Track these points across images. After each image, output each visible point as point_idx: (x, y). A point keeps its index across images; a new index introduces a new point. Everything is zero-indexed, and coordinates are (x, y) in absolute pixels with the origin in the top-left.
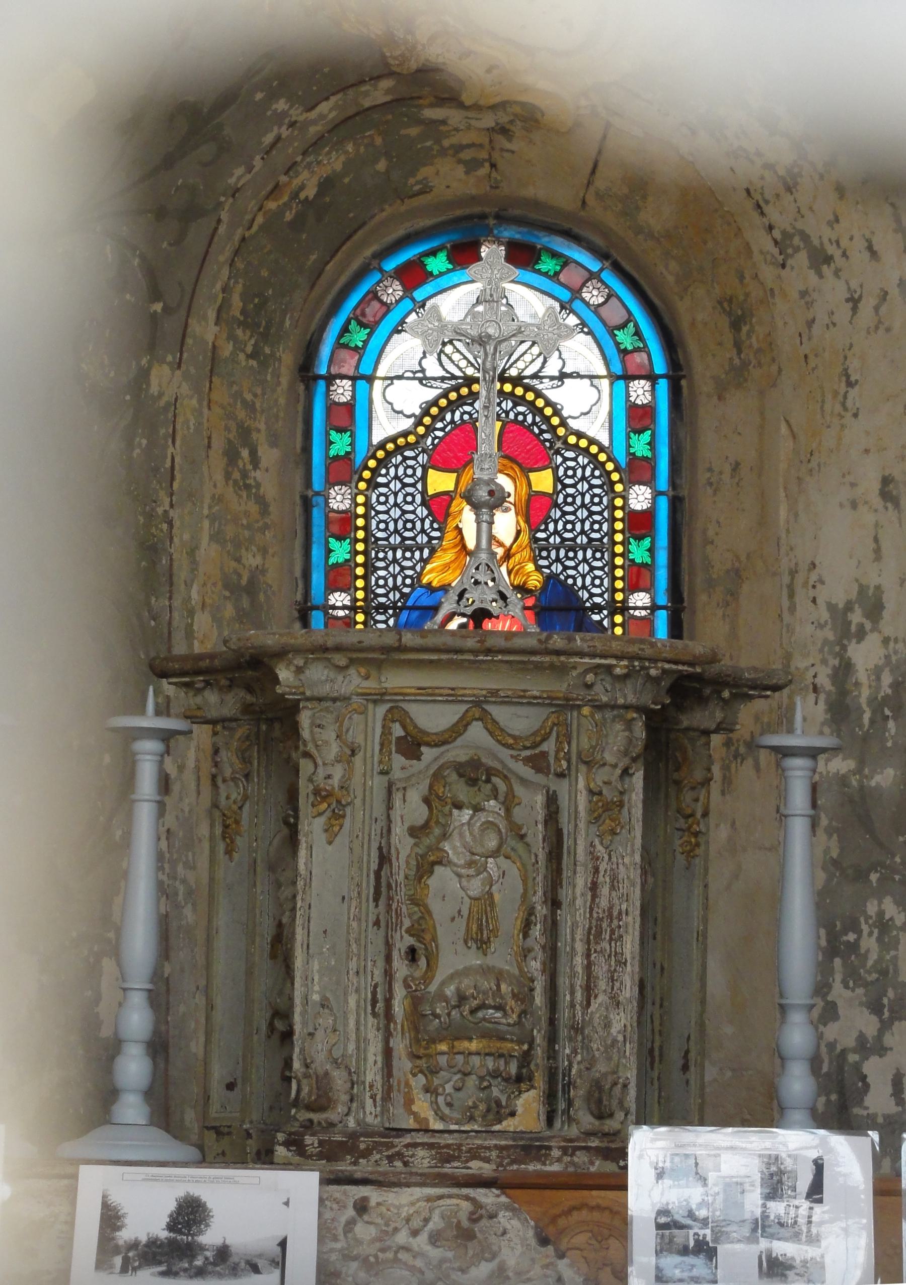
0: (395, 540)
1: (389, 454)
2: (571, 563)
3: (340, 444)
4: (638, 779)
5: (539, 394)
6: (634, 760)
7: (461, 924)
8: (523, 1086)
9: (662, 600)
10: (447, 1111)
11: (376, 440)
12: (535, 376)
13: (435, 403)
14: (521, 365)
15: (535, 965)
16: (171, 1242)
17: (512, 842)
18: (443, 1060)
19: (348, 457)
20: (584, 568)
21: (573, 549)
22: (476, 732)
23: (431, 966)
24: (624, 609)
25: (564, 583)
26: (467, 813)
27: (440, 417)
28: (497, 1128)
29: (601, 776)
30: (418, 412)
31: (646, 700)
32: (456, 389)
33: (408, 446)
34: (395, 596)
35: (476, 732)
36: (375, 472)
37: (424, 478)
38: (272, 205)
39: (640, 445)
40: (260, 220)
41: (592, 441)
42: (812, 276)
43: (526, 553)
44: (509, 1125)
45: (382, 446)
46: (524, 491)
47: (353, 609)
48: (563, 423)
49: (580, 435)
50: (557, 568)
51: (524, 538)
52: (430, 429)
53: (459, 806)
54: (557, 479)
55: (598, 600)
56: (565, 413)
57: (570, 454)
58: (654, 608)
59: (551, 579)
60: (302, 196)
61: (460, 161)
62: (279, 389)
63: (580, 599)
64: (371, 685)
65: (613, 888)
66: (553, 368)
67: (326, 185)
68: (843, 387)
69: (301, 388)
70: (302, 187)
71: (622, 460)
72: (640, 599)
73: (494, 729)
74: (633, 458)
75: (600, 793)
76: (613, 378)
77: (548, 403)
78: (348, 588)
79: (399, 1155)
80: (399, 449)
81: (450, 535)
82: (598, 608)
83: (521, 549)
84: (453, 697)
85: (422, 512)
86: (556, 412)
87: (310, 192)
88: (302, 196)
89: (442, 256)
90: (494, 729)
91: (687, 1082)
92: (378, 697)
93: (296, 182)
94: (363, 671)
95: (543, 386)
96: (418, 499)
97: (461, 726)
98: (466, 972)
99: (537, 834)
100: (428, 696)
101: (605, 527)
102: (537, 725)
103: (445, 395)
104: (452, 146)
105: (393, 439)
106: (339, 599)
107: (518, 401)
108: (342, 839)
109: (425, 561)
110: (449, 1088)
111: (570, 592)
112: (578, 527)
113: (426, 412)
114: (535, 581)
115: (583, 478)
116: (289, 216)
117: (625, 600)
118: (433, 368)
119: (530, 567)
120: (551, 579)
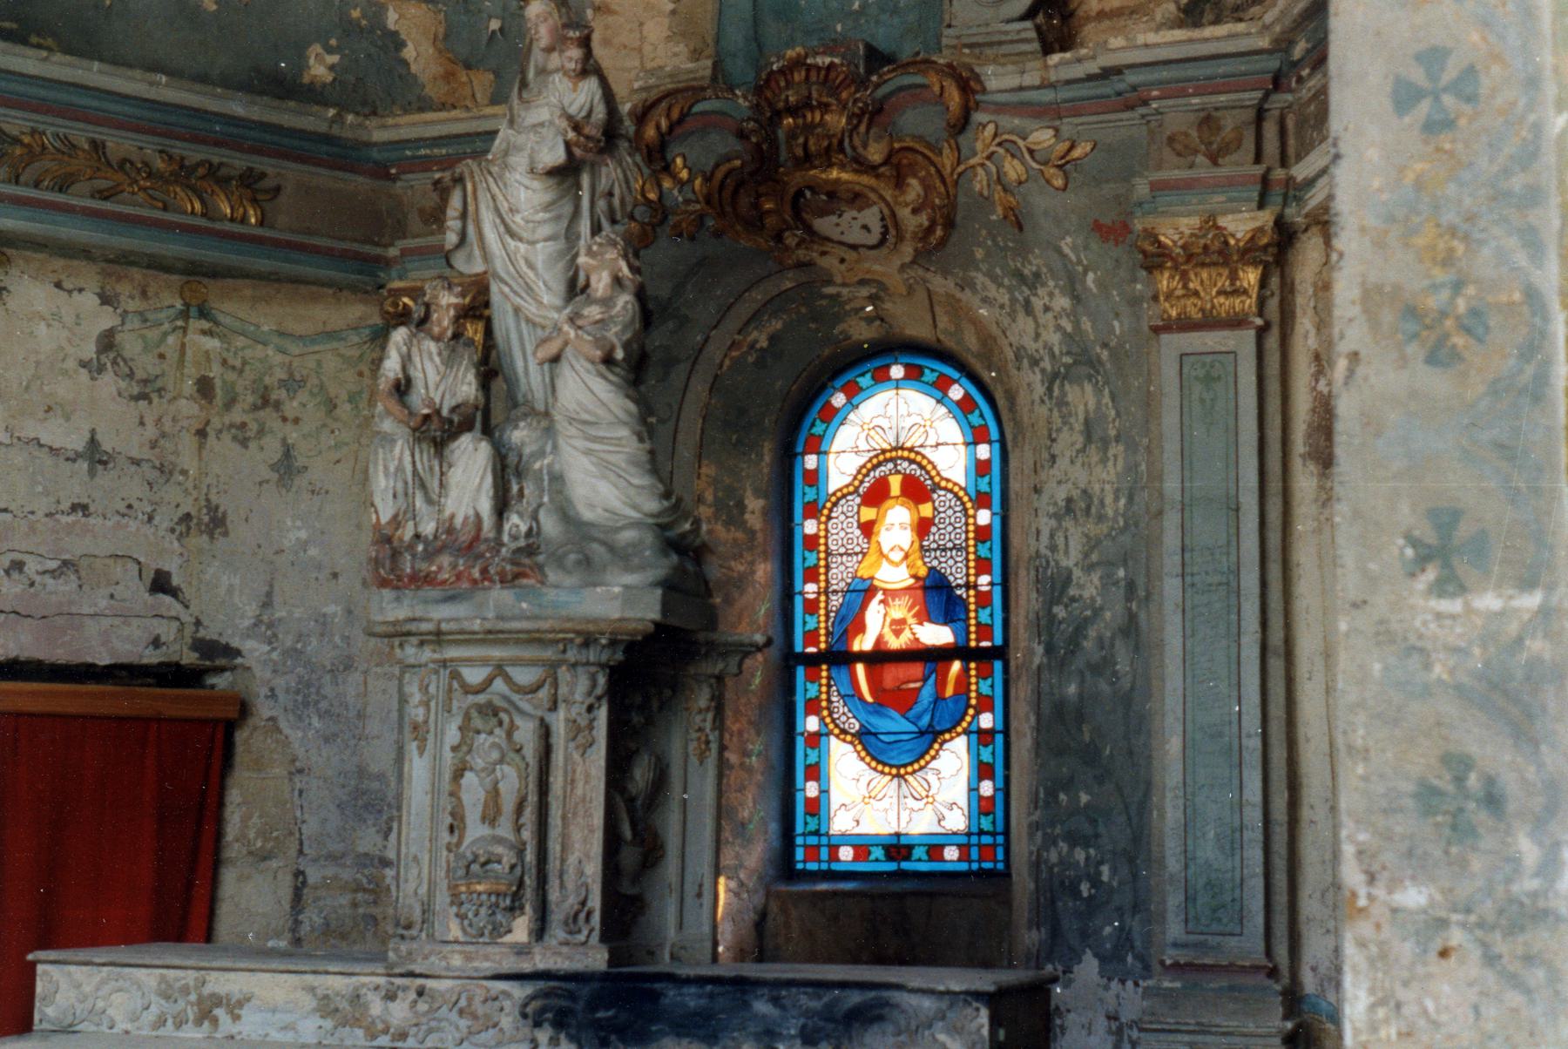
0: (842, 550)
1: (839, 499)
2: (943, 559)
3: (811, 494)
4: (602, 713)
5: (924, 457)
6: (599, 698)
7: (480, 808)
8: (518, 912)
9: (998, 580)
10: (469, 929)
11: (831, 491)
12: (921, 446)
13: (864, 466)
14: (913, 440)
15: (527, 834)
16: (606, 974)
17: (512, 755)
18: (463, 897)
19: (815, 502)
20: (951, 562)
21: (944, 550)
22: (499, 685)
23: (461, 838)
24: (975, 586)
25: (939, 572)
26: (483, 736)
27: (867, 475)
28: (499, 940)
29: (575, 710)
30: (854, 472)
31: (604, 658)
32: (877, 456)
33: (850, 494)
34: (842, 584)
35: (499, 685)
36: (831, 510)
37: (858, 513)
38: (735, 354)
39: (983, 485)
40: (727, 362)
41: (955, 484)
42: (1031, 375)
43: (917, 554)
44: (508, 938)
45: (834, 494)
46: (916, 517)
47: (819, 593)
48: (938, 474)
49: (948, 480)
50: (935, 563)
51: (916, 545)
52: (862, 482)
53: (478, 732)
54: (935, 509)
55: (959, 582)
56: (939, 468)
57: (942, 493)
58: (991, 584)
59: (932, 569)
60: (758, 346)
61: (861, 318)
62: (763, 464)
63: (949, 581)
64: (437, 656)
65: (586, 782)
66: (932, 441)
67: (773, 339)
68: (1049, 443)
69: (436, 463)
70: (756, 341)
71: (973, 496)
72: (984, 580)
73: (508, 679)
74: (978, 493)
75: (575, 721)
76: (967, 444)
77: (930, 462)
78: (816, 581)
79: (445, 958)
80: (844, 496)
81: (874, 546)
82: (959, 586)
83: (914, 552)
84: (484, 662)
85: (858, 532)
86: (934, 467)
87: (763, 343)
88: (758, 346)
89: (868, 376)
90: (508, 679)
91: (701, 905)
92: (444, 663)
93: (750, 339)
94: (431, 647)
95: (926, 452)
96: (855, 525)
97: (489, 681)
98: (482, 839)
99: (530, 752)
100: (469, 661)
101: (963, 536)
102: (537, 677)
103: (870, 460)
104: (852, 309)
105: (840, 490)
106: (811, 588)
107: (912, 462)
108: (426, 754)
109: (860, 562)
110: (470, 915)
111: (943, 577)
112: (947, 537)
113: (859, 472)
114: (923, 572)
115: (950, 507)
116: (750, 359)
117: (976, 581)
118: (863, 446)
119: (920, 563)
120: (932, 569)
